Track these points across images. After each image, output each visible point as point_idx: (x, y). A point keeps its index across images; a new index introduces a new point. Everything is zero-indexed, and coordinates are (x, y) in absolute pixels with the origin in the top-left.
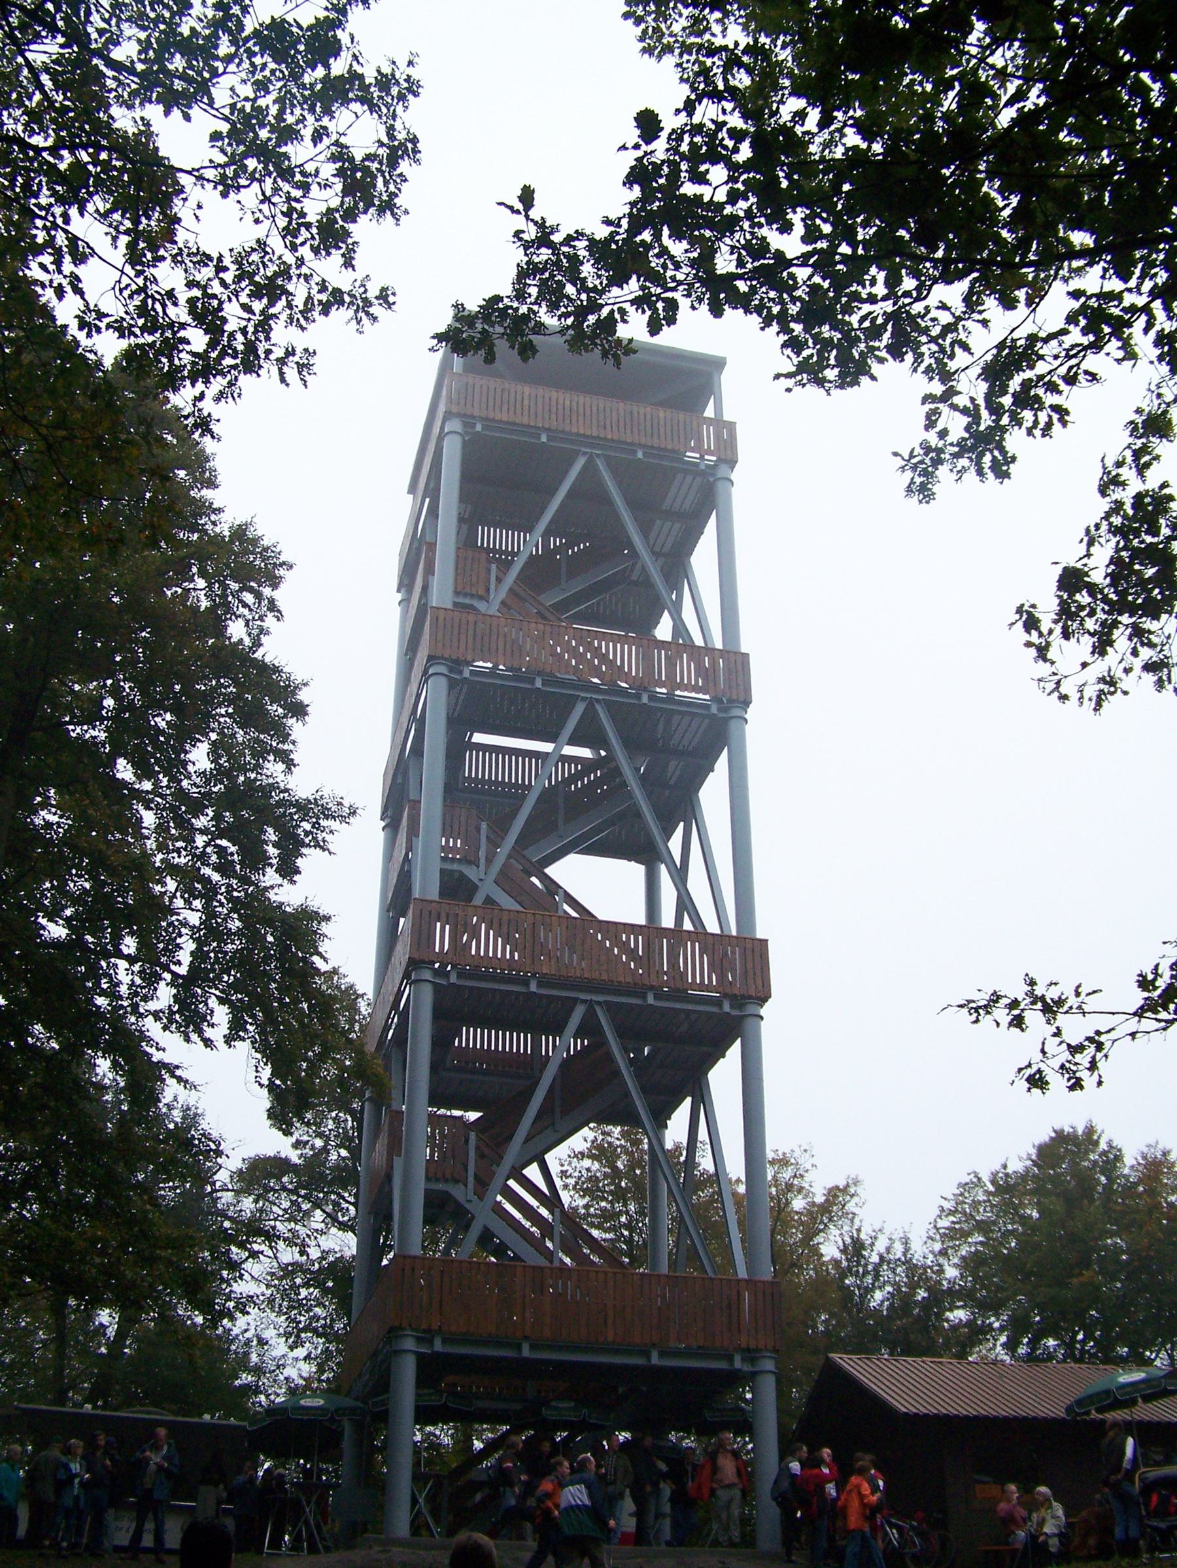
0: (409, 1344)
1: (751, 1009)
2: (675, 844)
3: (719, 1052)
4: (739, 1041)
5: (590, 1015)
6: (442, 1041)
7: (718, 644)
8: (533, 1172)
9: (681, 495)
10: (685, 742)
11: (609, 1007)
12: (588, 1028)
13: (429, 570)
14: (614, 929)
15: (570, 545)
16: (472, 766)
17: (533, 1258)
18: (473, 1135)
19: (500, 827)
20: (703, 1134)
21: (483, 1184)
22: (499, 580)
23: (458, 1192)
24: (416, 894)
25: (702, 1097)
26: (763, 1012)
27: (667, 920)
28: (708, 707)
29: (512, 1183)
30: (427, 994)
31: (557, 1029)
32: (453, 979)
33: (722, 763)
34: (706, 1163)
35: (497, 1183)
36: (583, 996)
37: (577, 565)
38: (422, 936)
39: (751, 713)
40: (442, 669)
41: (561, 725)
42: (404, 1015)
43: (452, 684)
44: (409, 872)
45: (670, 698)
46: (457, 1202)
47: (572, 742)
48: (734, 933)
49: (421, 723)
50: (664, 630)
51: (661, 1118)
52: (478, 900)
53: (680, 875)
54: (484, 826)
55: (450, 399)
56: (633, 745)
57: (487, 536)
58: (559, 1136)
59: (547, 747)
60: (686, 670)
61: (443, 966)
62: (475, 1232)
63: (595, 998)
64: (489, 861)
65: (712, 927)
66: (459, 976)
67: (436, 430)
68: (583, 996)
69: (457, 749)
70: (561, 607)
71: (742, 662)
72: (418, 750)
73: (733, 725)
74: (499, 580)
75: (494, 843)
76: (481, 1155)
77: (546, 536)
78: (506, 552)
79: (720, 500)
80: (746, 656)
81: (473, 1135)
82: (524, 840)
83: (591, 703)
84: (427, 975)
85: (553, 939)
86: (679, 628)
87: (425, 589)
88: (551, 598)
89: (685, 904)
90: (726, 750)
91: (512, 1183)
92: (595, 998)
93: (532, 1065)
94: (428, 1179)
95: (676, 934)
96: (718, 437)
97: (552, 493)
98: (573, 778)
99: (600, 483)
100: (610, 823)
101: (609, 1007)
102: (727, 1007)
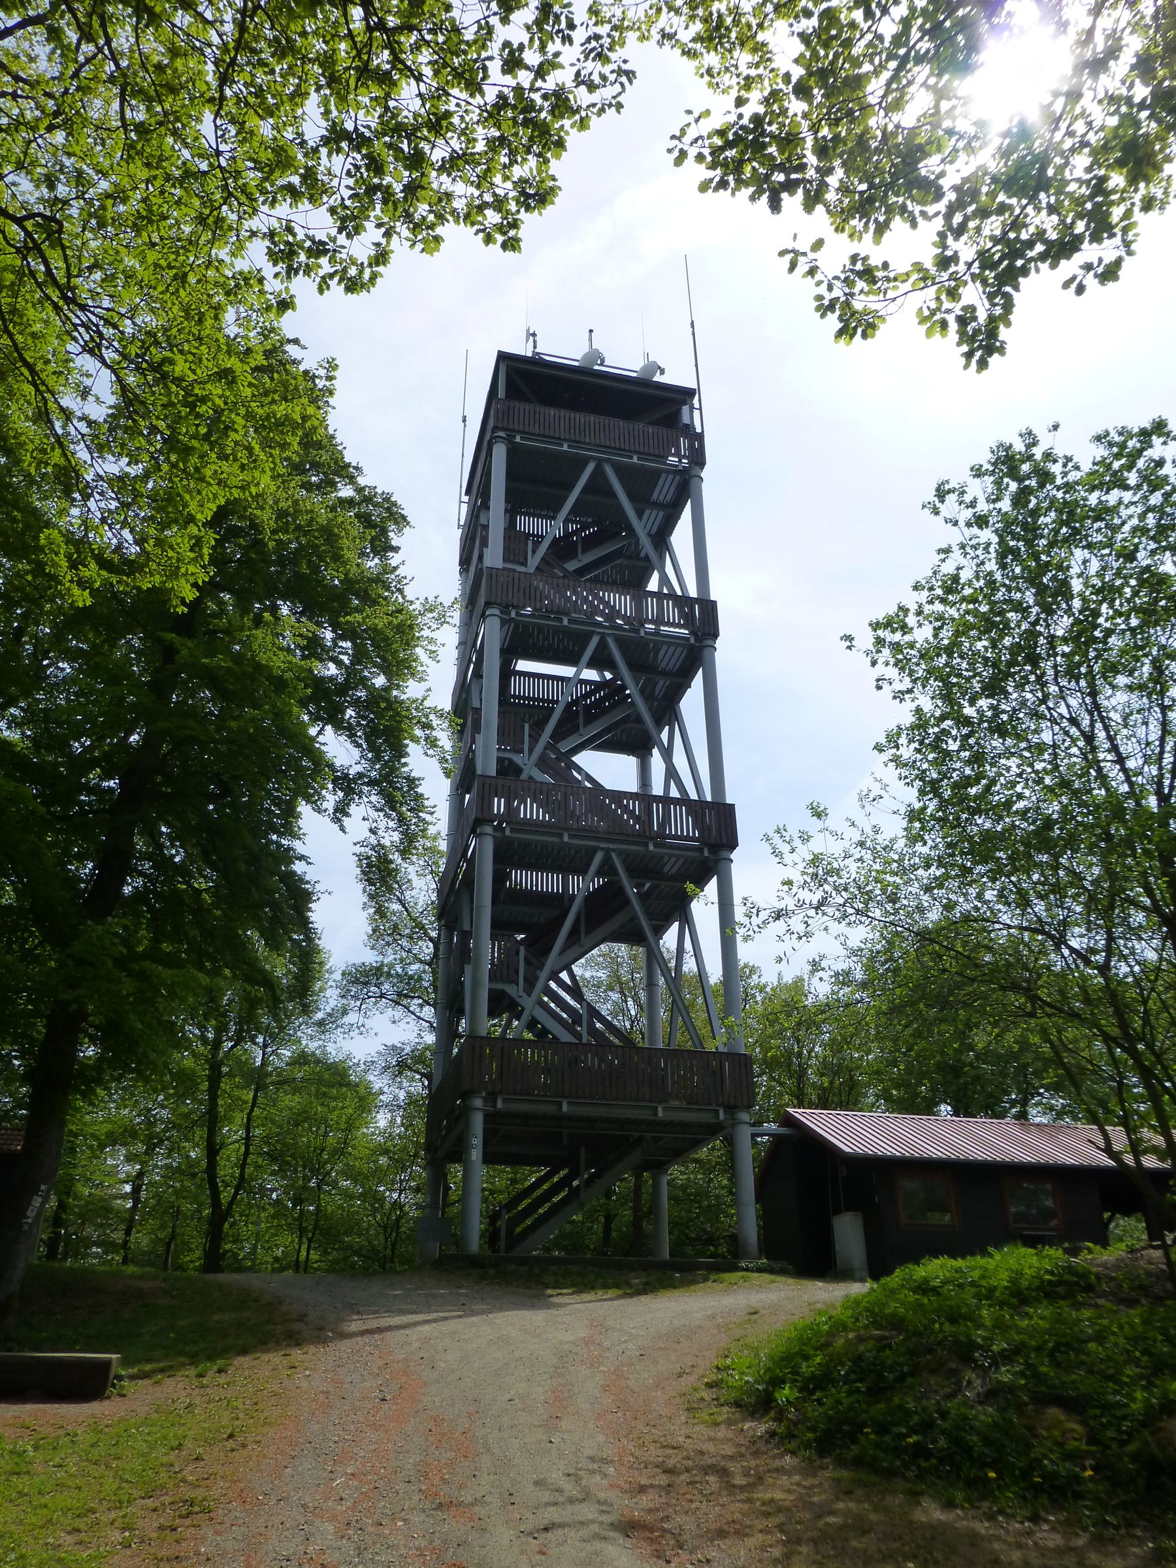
0: (478, 1102)
1: (724, 854)
2: (664, 736)
3: (701, 883)
4: (714, 880)
5: (607, 860)
6: (500, 878)
7: (693, 593)
8: (564, 975)
9: (663, 491)
10: (670, 666)
11: (620, 853)
12: (606, 869)
13: (484, 543)
14: (618, 796)
15: (583, 529)
16: (516, 687)
17: (565, 1037)
18: (522, 950)
19: (539, 726)
20: (688, 945)
21: (530, 983)
22: (534, 552)
23: (511, 990)
24: (479, 772)
25: (686, 920)
26: (732, 856)
27: (657, 789)
28: (687, 639)
29: (553, 985)
30: (489, 845)
31: (582, 871)
32: (508, 833)
33: (698, 681)
34: (690, 965)
35: (539, 985)
36: (603, 845)
37: (590, 543)
38: (484, 802)
39: (719, 643)
40: (496, 611)
41: (588, 866)
42: (471, 862)
43: (503, 623)
44: (473, 759)
45: (657, 633)
46: (510, 998)
47: (590, 665)
48: (709, 799)
49: (480, 653)
50: (653, 585)
51: (660, 931)
52: (524, 776)
53: (667, 754)
54: (527, 726)
55: (497, 417)
56: (633, 667)
57: (526, 524)
58: (582, 950)
59: (567, 671)
60: (672, 612)
61: (500, 824)
62: (525, 1017)
63: (611, 846)
64: (531, 750)
65: (693, 796)
66: (512, 830)
67: (487, 437)
68: (603, 845)
69: (507, 673)
70: (581, 572)
71: (709, 608)
72: (478, 675)
73: (706, 651)
74: (534, 552)
75: (534, 739)
76: (528, 962)
77: (566, 521)
78: (548, 701)
79: (693, 491)
80: (714, 603)
81: (522, 950)
82: (558, 736)
83: (603, 636)
84: (488, 829)
85: (578, 805)
86: (664, 580)
87: (481, 557)
88: (572, 566)
89: (671, 773)
90: (700, 674)
91: (553, 985)
92: (611, 846)
93: (561, 902)
94: (490, 980)
95: (666, 800)
96: (691, 446)
97: (571, 487)
98: (592, 692)
99: (610, 654)
100: (615, 725)
101: (620, 853)
102: (706, 853)
